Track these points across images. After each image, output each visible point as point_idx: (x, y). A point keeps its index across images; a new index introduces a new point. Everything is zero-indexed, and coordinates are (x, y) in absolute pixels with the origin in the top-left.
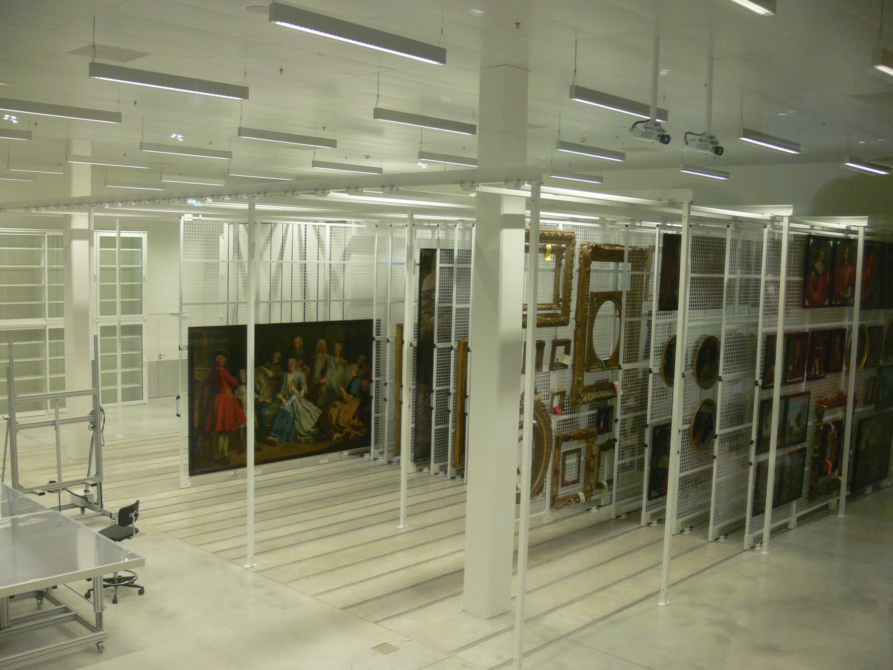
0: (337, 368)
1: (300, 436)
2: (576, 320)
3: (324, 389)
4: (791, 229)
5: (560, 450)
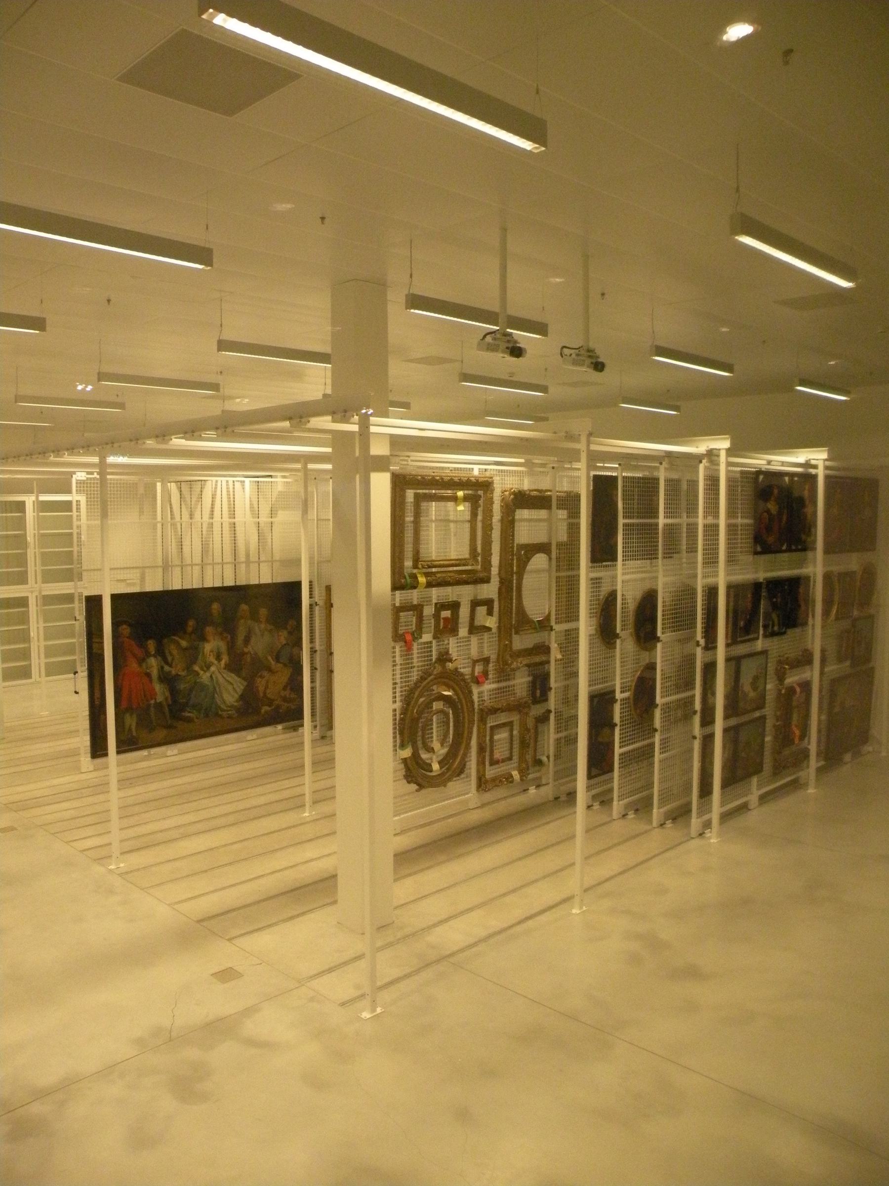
0: (262, 635)
1: (222, 711)
2: (500, 577)
3: (248, 658)
4: (729, 464)
5: (485, 724)
